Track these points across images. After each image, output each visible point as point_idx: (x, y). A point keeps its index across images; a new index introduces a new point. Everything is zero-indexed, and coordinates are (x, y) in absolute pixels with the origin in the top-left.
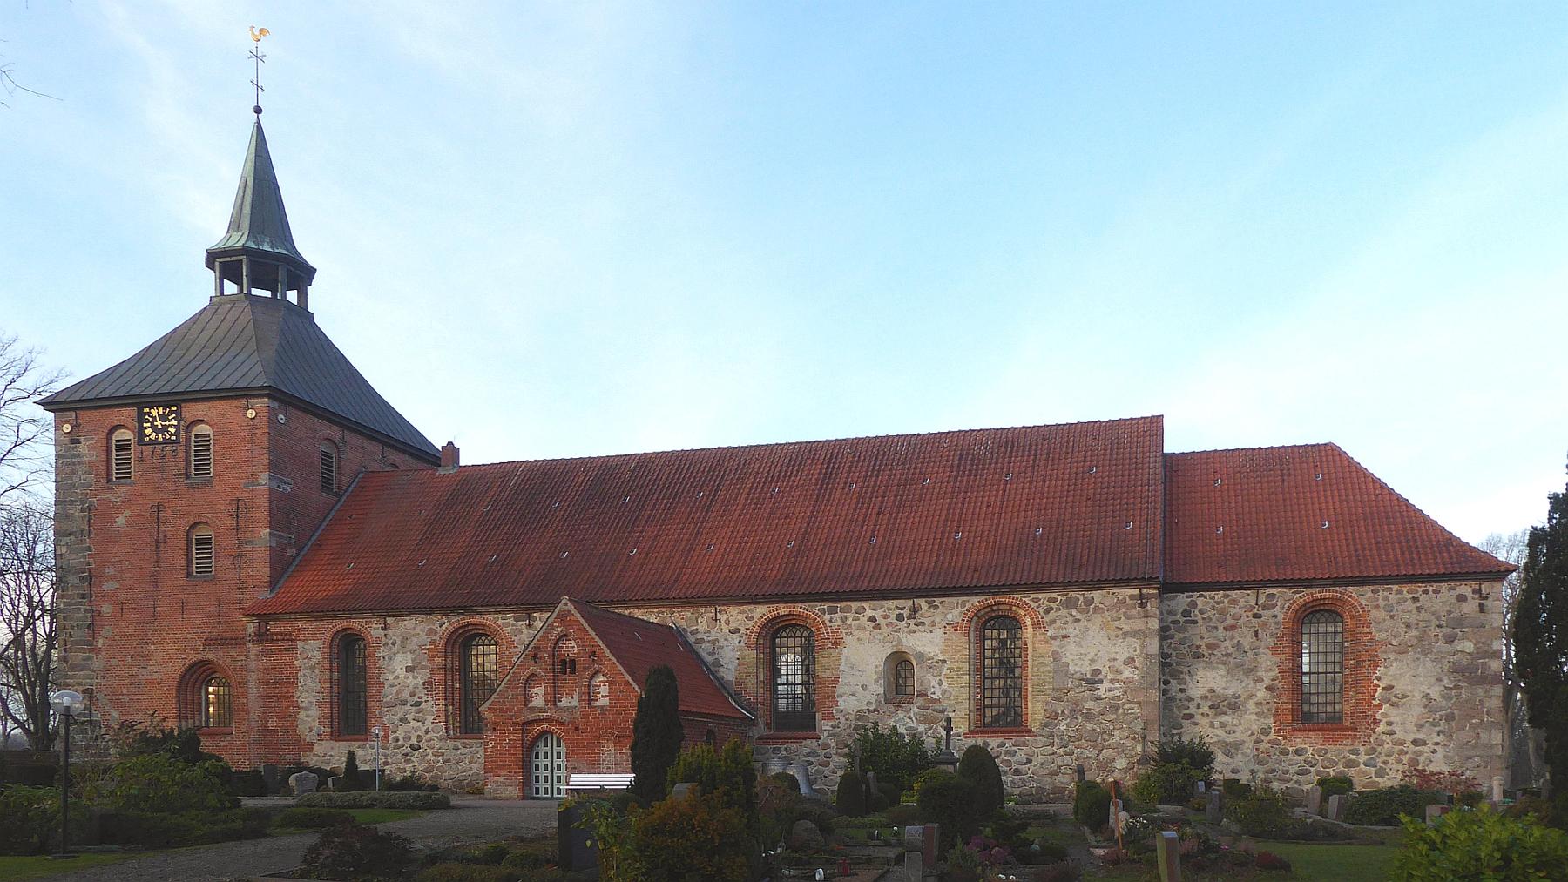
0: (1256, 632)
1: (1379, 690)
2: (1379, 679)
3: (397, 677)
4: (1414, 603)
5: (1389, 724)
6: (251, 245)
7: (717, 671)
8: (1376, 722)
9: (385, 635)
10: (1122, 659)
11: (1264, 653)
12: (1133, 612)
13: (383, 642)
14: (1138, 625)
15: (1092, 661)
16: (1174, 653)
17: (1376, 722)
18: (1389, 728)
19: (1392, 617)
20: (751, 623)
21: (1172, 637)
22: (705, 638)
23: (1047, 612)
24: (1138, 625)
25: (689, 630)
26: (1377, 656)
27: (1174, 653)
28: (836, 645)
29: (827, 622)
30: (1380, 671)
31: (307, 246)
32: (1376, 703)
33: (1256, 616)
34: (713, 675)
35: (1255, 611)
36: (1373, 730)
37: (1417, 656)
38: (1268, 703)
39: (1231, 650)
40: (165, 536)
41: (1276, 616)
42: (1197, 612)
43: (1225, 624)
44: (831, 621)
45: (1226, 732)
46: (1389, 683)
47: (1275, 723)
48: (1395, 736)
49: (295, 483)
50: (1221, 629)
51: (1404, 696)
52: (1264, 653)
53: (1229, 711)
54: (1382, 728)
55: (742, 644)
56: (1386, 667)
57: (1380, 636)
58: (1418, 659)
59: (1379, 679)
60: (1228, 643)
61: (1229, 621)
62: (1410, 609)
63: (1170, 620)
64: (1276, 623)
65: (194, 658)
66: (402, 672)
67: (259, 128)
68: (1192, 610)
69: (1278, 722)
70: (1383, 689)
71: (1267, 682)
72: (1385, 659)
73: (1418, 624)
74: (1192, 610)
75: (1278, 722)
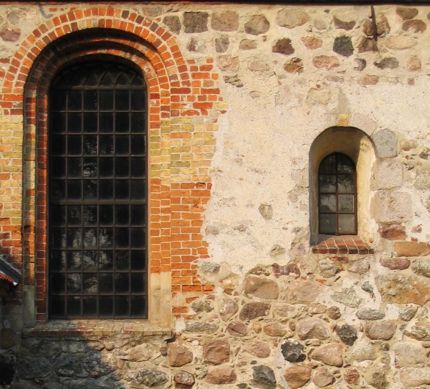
28: (203, 107)
29: (183, 50)
44: (192, 48)
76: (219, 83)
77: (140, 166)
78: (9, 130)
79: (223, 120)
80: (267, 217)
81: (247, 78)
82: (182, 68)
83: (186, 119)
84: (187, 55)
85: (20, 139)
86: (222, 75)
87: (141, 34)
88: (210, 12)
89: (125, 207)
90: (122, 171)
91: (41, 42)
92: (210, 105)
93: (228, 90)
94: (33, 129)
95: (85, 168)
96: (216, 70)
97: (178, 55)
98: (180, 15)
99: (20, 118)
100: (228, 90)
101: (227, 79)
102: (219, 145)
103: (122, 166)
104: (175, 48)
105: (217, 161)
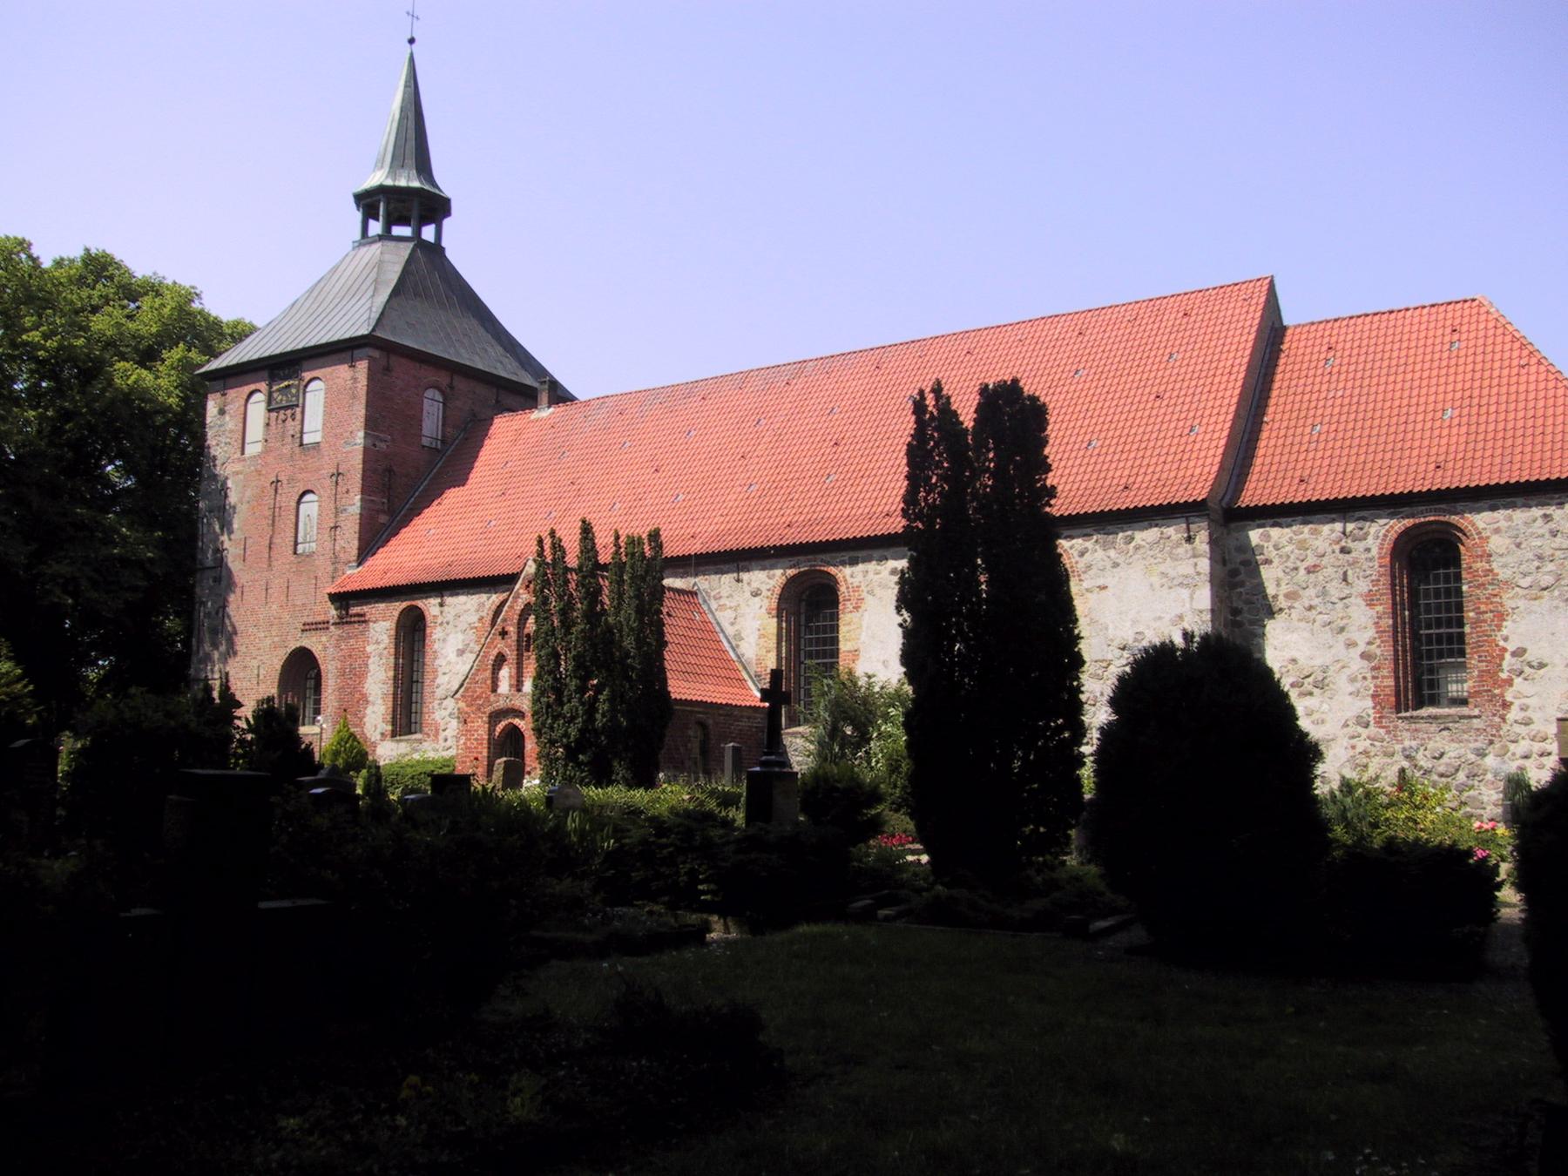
0: (1345, 573)
1: (1507, 656)
2: (1506, 639)
3: (449, 663)
4: (628, 536)
5: (1524, 708)
6: (389, 182)
7: (738, 646)
8: (1506, 705)
9: (442, 612)
10: (1167, 617)
11: (1356, 605)
12: (1180, 550)
13: (439, 621)
14: (1186, 568)
15: (1135, 622)
16: (1246, 608)
17: (1506, 705)
18: (1523, 714)
19: (1518, 545)
20: (772, 582)
21: (1242, 584)
22: (727, 603)
23: (1082, 554)
24: (1186, 568)
25: (712, 594)
26: (1501, 605)
27: (1246, 608)
28: (857, 608)
29: (848, 578)
30: (1508, 627)
31: (447, 180)
32: (1504, 675)
33: (1344, 551)
34: (734, 650)
35: (1343, 544)
36: (1503, 719)
37: (1555, 603)
38: (1365, 678)
39: (1316, 601)
40: (280, 508)
41: (1368, 550)
42: (1271, 548)
43: (1306, 564)
44: (852, 576)
45: (1313, 722)
46: (1520, 645)
47: (1374, 708)
48: (1532, 726)
49: (393, 440)
50: (1302, 572)
51: (1542, 666)
52: (1356, 605)
53: (1316, 691)
54: (1514, 714)
55: (763, 610)
56: (1514, 621)
57: (1504, 575)
58: (1557, 607)
59: (1506, 639)
60: (1311, 592)
61: (1311, 561)
62: (1540, 532)
63: (1238, 561)
64: (1371, 560)
65: (293, 645)
66: (452, 656)
67: (412, 60)
68: (1266, 545)
69: (1378, 707)
70: (1514, 654)
71: (1362, 647)
72: (1513, 609)
73: (1553, 555)
74: (1266, 545)
75: (1378, 707)
76: (864, 595)
77: (835, 641)
78: (1547, 580)
79: (866, 614)
80: (886, 667)
81: (877, 591)
82: (848, 588)
83: (850, 615)
84: (850, 580)
85: (775, 631)
86: (865, 590)
87: (1466, 531)
88: (860, 555)
89: (1448, 627)
90: (1448, 610)
91: (1388, 545)
92: (860, 607)
93: (869, 598)
94: (784, 625)
95: (91, 682)
96: (863, 587)
97: (845, 581)
98: (846, 558)
99: (775, 620)
100: (869, 598)
101: (868, 592)
102: (864, 629)
103: (825, 642)
104: (844, 577)
105: (863, 637)
